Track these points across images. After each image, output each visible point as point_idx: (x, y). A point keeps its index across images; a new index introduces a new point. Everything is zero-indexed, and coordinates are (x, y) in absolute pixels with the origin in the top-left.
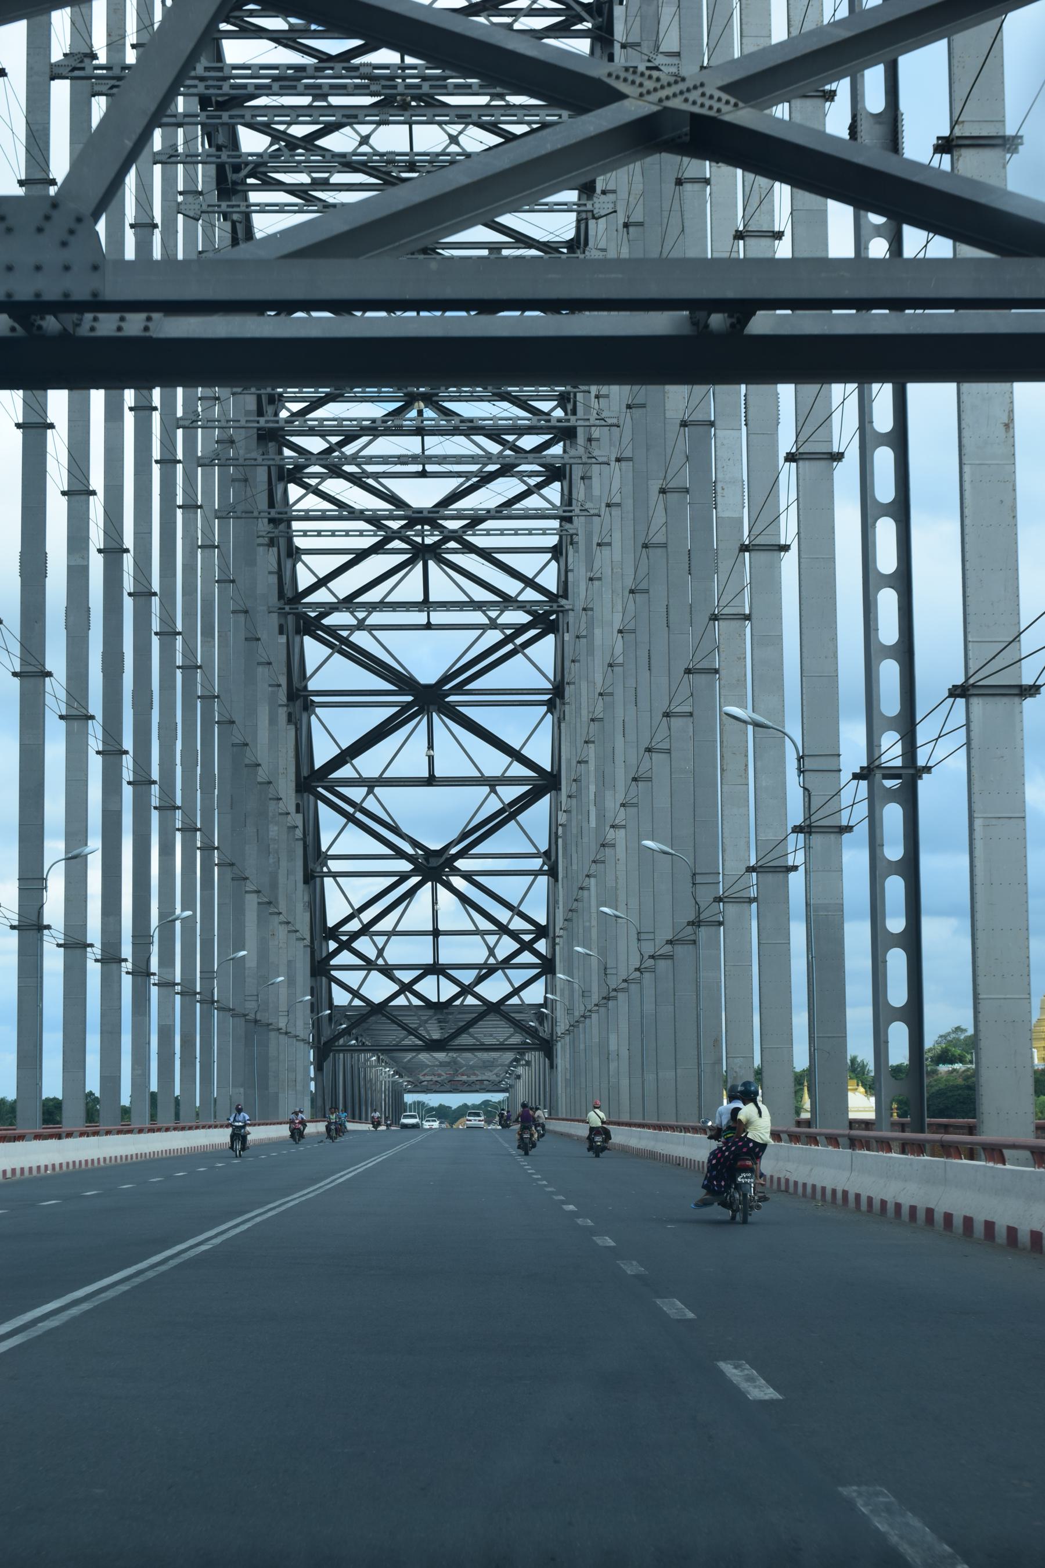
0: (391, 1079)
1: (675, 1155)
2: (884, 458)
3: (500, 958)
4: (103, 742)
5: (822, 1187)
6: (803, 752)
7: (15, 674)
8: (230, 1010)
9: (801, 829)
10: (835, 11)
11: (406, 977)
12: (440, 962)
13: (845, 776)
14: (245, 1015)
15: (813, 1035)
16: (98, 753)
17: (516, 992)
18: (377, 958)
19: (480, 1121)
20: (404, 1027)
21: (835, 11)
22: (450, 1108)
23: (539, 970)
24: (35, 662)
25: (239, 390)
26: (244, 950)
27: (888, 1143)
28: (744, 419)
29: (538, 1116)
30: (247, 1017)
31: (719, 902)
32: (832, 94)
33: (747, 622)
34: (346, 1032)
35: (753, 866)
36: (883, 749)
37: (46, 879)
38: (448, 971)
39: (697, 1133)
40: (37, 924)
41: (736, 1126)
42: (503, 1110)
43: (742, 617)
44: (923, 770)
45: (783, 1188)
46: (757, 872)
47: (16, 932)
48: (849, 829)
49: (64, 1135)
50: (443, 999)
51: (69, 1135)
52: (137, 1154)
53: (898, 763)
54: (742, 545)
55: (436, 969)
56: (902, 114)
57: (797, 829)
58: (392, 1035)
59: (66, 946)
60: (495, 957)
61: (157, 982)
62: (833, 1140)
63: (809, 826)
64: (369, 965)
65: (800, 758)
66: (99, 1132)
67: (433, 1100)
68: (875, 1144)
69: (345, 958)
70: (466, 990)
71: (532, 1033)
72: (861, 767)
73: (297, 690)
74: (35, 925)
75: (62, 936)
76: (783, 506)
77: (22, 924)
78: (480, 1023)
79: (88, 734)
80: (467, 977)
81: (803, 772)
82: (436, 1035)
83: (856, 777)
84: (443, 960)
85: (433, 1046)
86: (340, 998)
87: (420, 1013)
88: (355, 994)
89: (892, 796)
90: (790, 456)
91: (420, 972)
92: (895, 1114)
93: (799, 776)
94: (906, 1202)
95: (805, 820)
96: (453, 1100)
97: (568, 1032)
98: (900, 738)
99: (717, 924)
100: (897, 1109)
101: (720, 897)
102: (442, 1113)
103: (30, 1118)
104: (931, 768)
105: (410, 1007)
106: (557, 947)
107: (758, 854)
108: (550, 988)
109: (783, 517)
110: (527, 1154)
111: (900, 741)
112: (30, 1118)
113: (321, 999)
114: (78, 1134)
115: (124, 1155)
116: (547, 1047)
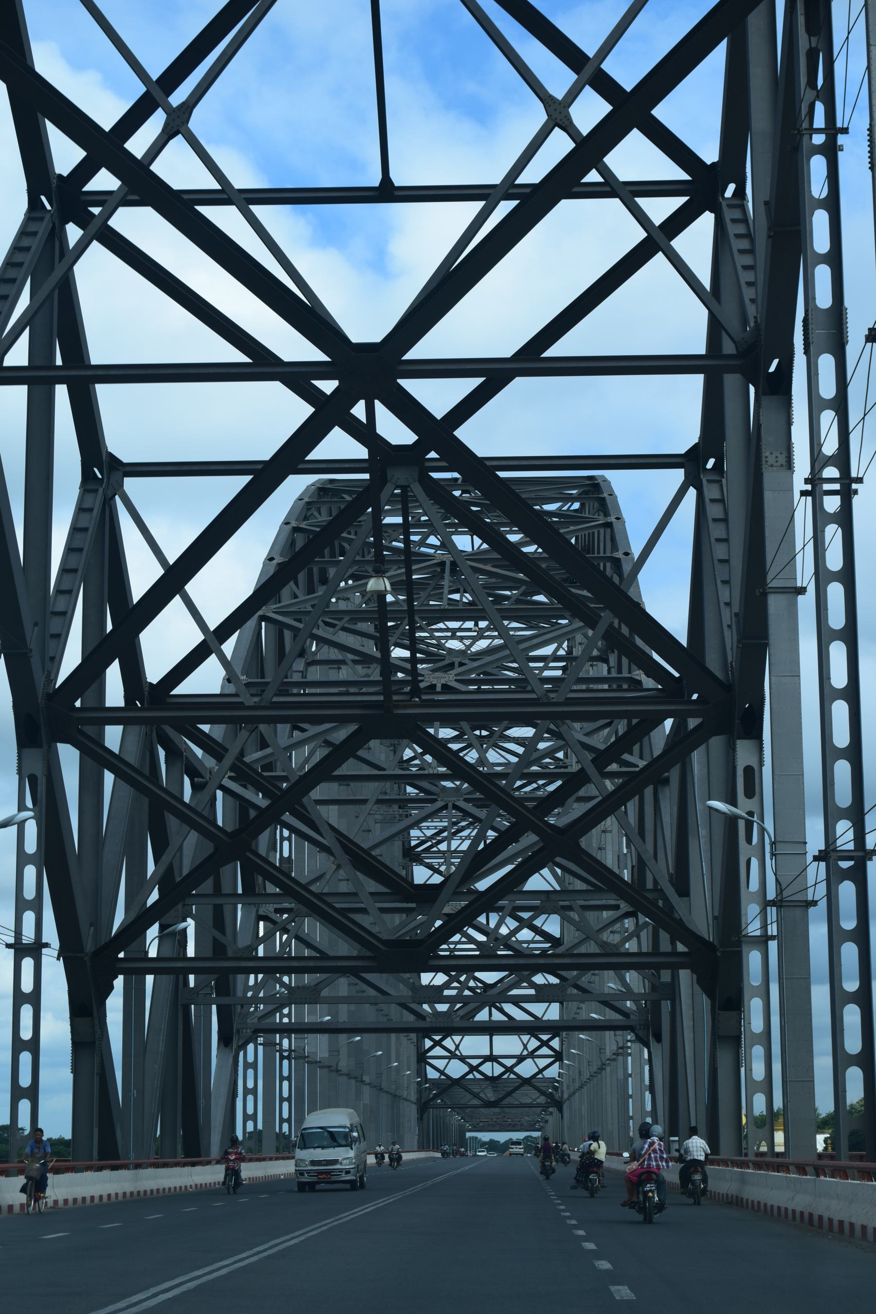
0: (458, 1123)
1: (776, 1205)
2: (836, 592)
3: (530, 1049)
5: (793, 1210)
6: (775, 839)
8: (317, 1062)
9: (773, 903)
11: (475, 1062)
12: (494, 1054)
13: (810, 858)
14: (329, 1067)
15: (785, 1080)
18: (455, 1050)
19: (520, 1149)
20: (471, 1093)
22: (499, 1142)
23: (553, 1059)
27: (845, 1171)
29: (565, 1149)
34: (436, 1096)
36: (838, 834)
39: (760, 1169)
41: (592, 1153)
42: (538, 1144)
43: (793, 590)
44: (872, 853)
45: (756, 1208)
50: (496, 1074)
53: (851, 846)
55: (491, 1058)
56: (846, 309)
60: (527, 1050)
61: (262, 1042)
62: (801, 1169)
63: (781, 901)
64: (452, 1055)
68: (764, 1165)
69: (438, 1051)
70: (509, 1070)
72: (819, 851)
76: (799, 546)
78: (517, 1092)
80: (509, 1062)
81: (775, 855)
82: (492, 1099)
83: (816, 859)
84: (496, 1052)
85: (489, 1104)
86: (432, 1074)
87: (481, 1083)
88: (442, 1072)
89: (846, 875)
91: (482, 1060)
92: (830, 1148)
94: (858, 1221)
95: (777, 896)
96: (501, 1137)
97: (568, 1099)
98: (851, 825)
99: (804, 904)
100: (831, 1144)
102: (492, 1146)
104: (817, 901)
105: (475, 1079)
106: (564, 1046)
108: (561, 1067)
110: (548, 1178)
111: (852, 828)
113: (422, 1073)
115: (105, 1194)
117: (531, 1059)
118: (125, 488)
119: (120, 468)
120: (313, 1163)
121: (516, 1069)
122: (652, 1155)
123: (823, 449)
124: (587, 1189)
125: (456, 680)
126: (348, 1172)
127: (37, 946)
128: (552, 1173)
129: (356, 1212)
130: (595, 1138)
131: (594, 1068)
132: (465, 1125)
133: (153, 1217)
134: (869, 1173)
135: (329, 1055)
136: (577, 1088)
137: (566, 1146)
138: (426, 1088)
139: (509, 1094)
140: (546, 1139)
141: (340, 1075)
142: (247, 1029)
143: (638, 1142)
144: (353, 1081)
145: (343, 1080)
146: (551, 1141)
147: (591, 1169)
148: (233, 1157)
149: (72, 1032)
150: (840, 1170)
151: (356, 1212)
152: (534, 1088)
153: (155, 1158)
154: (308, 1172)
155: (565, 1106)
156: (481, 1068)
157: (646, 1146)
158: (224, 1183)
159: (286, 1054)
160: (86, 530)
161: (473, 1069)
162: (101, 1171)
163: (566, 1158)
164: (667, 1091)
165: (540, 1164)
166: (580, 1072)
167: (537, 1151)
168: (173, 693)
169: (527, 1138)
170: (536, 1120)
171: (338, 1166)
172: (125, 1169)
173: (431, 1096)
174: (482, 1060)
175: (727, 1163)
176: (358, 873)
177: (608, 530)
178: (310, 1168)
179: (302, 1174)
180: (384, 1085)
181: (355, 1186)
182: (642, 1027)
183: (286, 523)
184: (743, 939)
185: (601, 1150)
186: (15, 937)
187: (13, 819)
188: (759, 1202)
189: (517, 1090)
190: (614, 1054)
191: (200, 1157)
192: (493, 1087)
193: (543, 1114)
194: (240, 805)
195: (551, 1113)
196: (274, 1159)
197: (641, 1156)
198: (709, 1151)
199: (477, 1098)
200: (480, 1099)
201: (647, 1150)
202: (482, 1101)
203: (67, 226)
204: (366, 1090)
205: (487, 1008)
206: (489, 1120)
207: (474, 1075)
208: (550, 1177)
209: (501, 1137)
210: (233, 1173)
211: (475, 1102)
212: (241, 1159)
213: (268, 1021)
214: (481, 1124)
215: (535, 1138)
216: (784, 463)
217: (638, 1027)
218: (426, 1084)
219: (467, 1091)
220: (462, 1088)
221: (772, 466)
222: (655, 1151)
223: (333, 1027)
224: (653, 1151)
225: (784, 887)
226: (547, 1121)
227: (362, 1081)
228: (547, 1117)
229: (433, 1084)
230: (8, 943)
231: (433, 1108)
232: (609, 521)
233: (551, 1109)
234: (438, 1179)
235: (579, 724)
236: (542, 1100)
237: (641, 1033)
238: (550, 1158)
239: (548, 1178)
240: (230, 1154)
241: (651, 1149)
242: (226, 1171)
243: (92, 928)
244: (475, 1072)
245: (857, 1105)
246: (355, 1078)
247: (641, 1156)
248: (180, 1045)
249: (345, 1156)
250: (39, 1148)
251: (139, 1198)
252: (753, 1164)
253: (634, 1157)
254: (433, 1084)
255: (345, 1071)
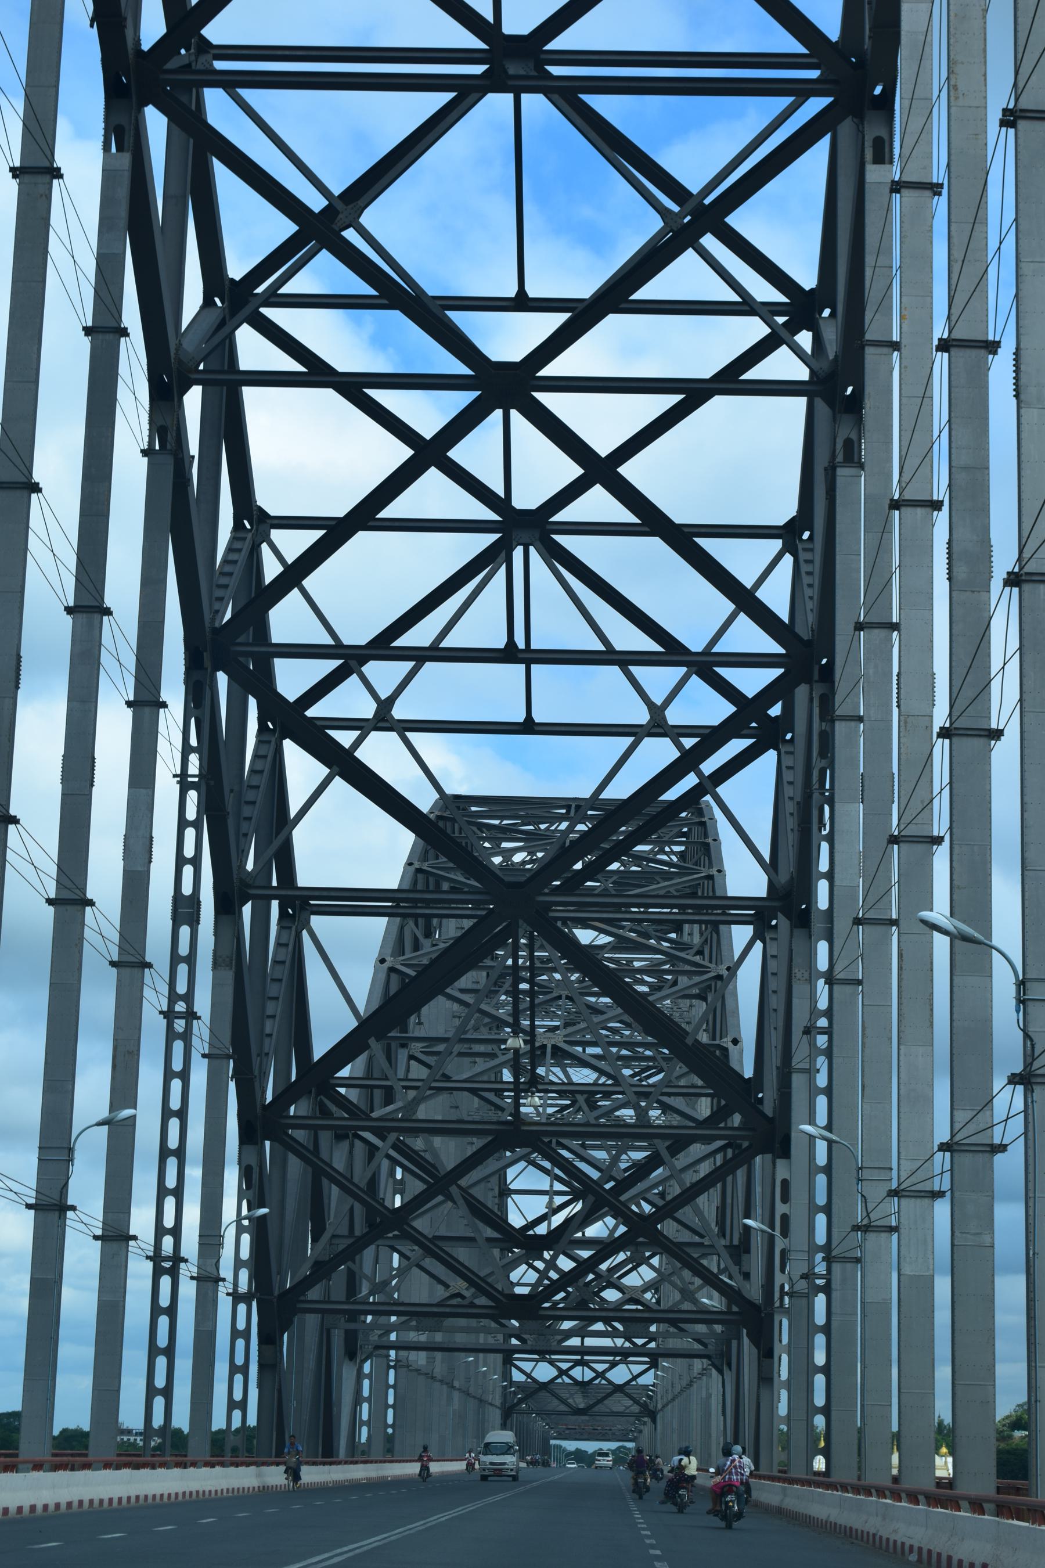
4: (210, 1044)
7: (113, 964)
9: (948, 1147)
10: (1001, 243)
16: (204, 1056)
17: (635, 1378)
19: (608, 1461)
21: (999, 248)
23: (648, 1366)
24: (132, 952)
25: (488, 1059)
26: (264, 1207)
27: (957, 1502)
28: (896, 691)
29: (658, 1463)
30: (410, 1368)
31: (857, 1231)
32: (939, 504)
33: (894, 928)
34: (521, 1401)
35: (895, 1190)
37: (223, 1237)
38: (590, 1364)
40: (58, 1203)
41: (681, 1468)
46: (899, 1198)
47: (195, 1282)
48: (1002, 1148)
49: (189, 1464)
50: (586, 1379)
51: (194, 1464)
52: (238, 1489)
54: (892, 836)
57: (944, 1147)
58: (555, 1404)
59: (38, 1207)
65: (1021, 984)
66: (196, 1463)
67: (571, 1445)
71: (644, 1406)
73: (503, 1190)
74: (56, 1205)
75: (34, 1194)
77: (39, 1202)
79: (143, 983)
82: (582, 1406)
86: (517, 1376)
88: (528, 1376)
90: (944, 731)
93: (1018, 1011)
96: (590, 1446)
97: (661, 1410)
101: (858, 1225)
102: (579, 1456)
103: (198, 1448)
105: (564, 1383)
107: (956, 1118)
108: (656, 1377)
109: (936, 802)
112: (198, 1448)
113: (507, 1376)
114: (203, 1463)
115: (180, 1491)
116: (653, 1415)
117: (624, 1365)
118: (311, 924)
119: (308, 908)
120: (492, 1464)
121: (608, 1375)
122: (733, 1470)
123: (818, 1005)
124: (675, 1504)
125: (565, 1041)
126: (512, 1470)
127: (249, 1295)
128: (646, 1492)
129: (454, 1513)
130: (687, 1453)
131: (684, 1383)
132: (549, 1432)
133: (110, 1536)
134: (858, 1489)
135: (427, 1362)
136: (685, 1386)
137: (659, 1460)
138: (511, 1392)
139: (600, 1401)
140: (639, 1451)
141: (454, 1390)
142: (368, 1345)
143: (721, 1460)
144: (445, 1386)
145: (437, 1385)
146: (645, 1453)
147: (680, 1485)
148: (425, 1459)
149: (259, 1356)
150: (951, 1500)
151: (454, 1513)
152: (625, 1395)
153: (246, 1457)
154: (488, 1469)
155: (659, 1417)
156: (571, 1373)
157: (729, 1463)
158: (420, 1475)
159: (392, 1364)
160: (283, 962)
161: (562, 1372)
162: (55, 1471)
163: (658, 1473)
164: (733, 1418)
165: (632, 1481)
166: (672, 1384)
167: (631, 1467)
168: (337, 1075)
169: (619, 1448)
170: (629, 1428)
171: (506, 1466)
172: (110, 1469)
173: (515, 1401)
174: (572, 1364)
175: (847, 1489)
176: (477, 1221)
177: (711, 882)
178: (489, 1466)
179: (484, 1470)
180: (472, 1390)
181: (515, 1478)
182: (718, 1356)
183: (409, 864)
184: (775, 1310)
185: (692, 1465)
186: (233, 1289)
187: (116, 1116)
188: (851, 1528)
189: (610, 1396)
190: (699, 1374)
191: (333, 1457)
192: (583, 1392)
193: (636, 1424)
194: (369, 1150)
195: (645, 1423)
196: (46, 1466)
197: (724, 1471)
198: (753, 1468)
199: (565, 1404)
200: (567, 1405)
201: (730, 1466)
202: (571, 1408)
203: (284, 741)
204: (456, 1395)
205: (498, 413)
206: (577, 1427)
207: (563, 1380)
208: (644, 1497)
209: (590, 1446)
210: (425, 1468)
211: (563, 1408)
212: (430, 1460)
213: (385, 1339)
214: (567, 1432)
215: (629, 1448)
216: (808, 978)
217: (714, 1356)
218: (511, 1388)
219: (553, 1396)
220: (549, 1392)
221: (799, 979)
222: (735, 1467)
223: (446, 1346)
224: (734, 1467)
225: (794, 1282)
226: (641, 1431)
227: (453, 1387)
228: (642, 1427)
229: (518, 1387)
230: (96, 1234)
231: (516, 1413)
232: (711, 873)
233: (646, 1419)
234: (534, 1484)
235: (688, 1000)
236: (636, 1409)
237: (716, 1362)
238: (644, 1473)
239: (641, 1498)
240: (424, 1456)
241: (733, 1465)
242: (421, 1467)
243: (279, 1276)
244: (564, 1377)
245: (999, 1424)
246: (447, 1384)
247: (724, 1471)
248: (324, 1362)
249: (510, 1460)
250: (293, 1448)
251: (91, 1509)
252: (907, 1495)
253: (718, 1473)
254: (518, 1387)
255: (439, 1377)
